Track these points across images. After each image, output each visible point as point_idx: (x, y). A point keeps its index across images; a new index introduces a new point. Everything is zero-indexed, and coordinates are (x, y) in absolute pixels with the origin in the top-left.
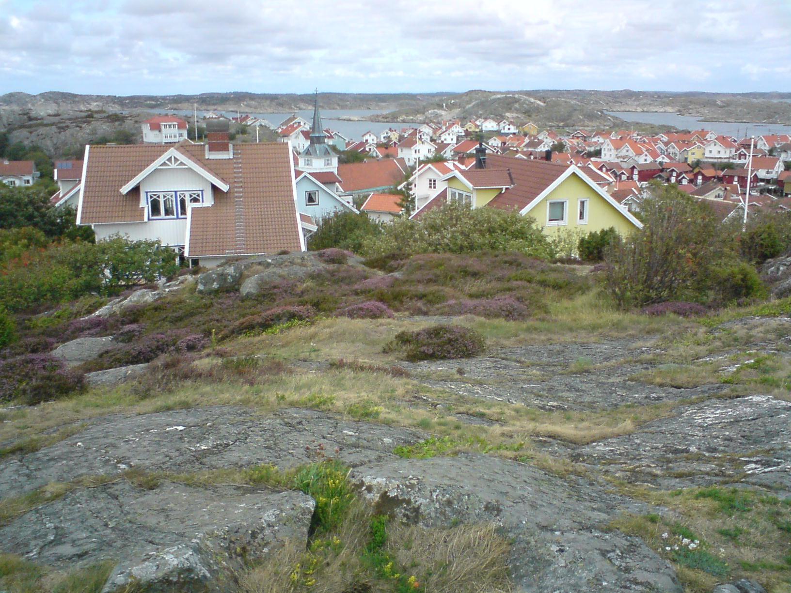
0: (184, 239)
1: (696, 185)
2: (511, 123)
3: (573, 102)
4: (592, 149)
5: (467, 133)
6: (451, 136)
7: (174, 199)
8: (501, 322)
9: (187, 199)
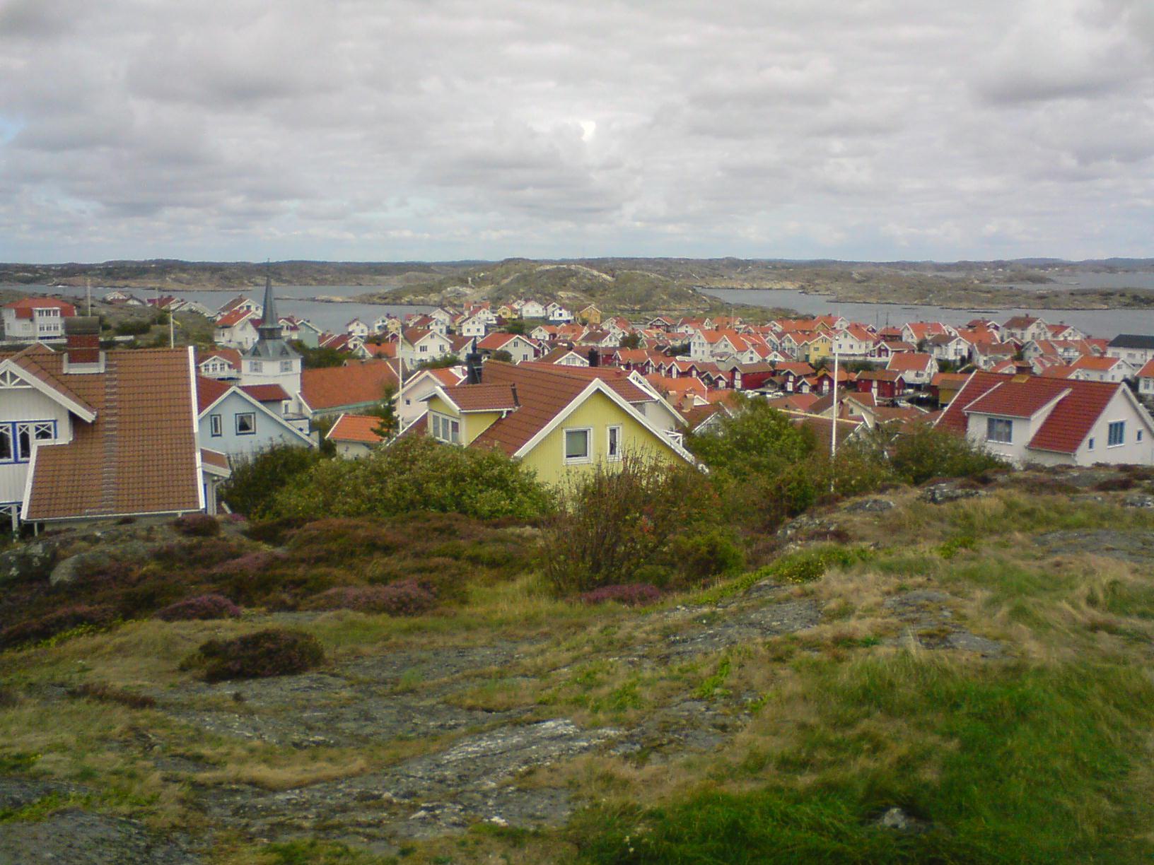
0: (22, 495)
1: (820, 393)
2: (563, 306)
3: (653, 276)
4: (678, 344)
5: (501, 321)
6: (477, 326)
7: (10, 434)
8: (382, 619)
9: (32, 434)
